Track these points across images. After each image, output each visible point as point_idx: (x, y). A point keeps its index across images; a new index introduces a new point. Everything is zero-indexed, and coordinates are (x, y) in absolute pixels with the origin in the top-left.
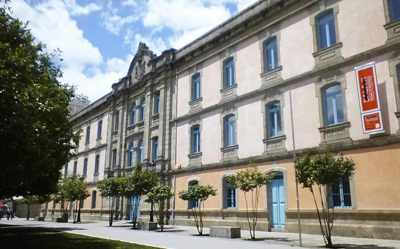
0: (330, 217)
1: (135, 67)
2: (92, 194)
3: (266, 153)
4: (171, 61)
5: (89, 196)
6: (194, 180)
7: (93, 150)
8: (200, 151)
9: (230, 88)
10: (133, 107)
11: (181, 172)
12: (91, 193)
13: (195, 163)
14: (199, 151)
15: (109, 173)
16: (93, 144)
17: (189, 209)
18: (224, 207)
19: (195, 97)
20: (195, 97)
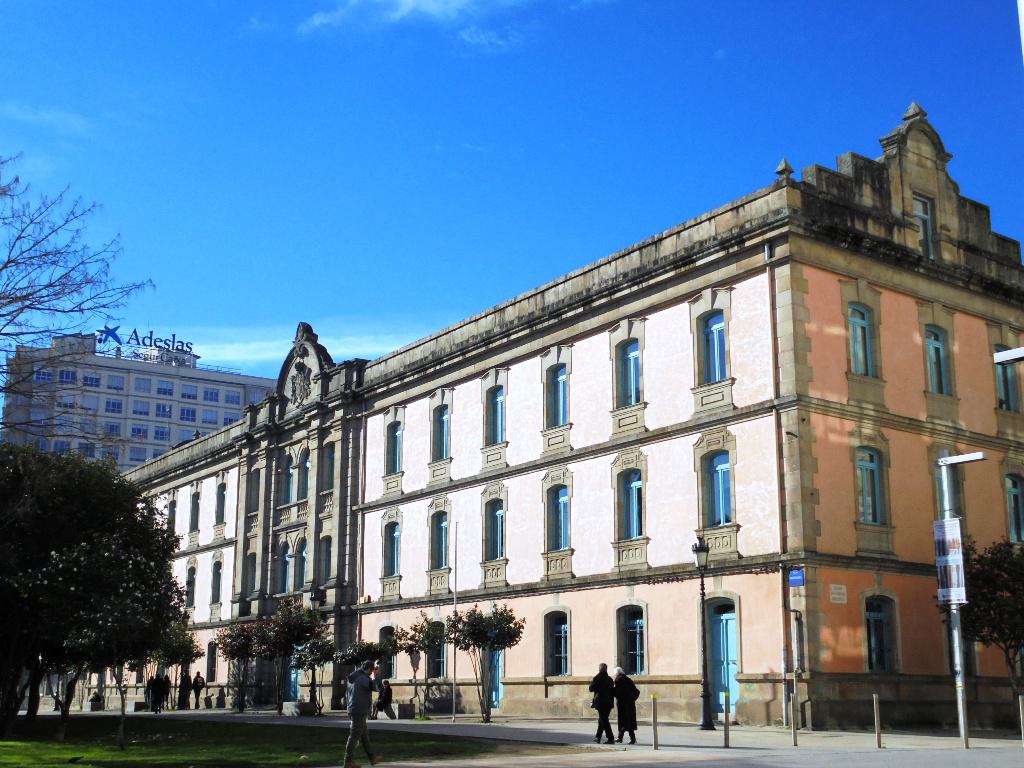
0: (548, 684)
1: (290, 376)
2: (206, 654)
3: (617, 570)
4: (353, 388)
5: (199, 655)
6: (632, 606)
7: (208, 548)
8: (644, 533)
9: (715, 386)
10: (288, 468)
11: (370, 608)
12: (205, 648)
13: (391, 595)
14: (640, 533)
15: (243, 601)
16: (206, 536)
17: (429, 677)
18: (547, 674)
19: (627, 394)
20: (627, 394)
